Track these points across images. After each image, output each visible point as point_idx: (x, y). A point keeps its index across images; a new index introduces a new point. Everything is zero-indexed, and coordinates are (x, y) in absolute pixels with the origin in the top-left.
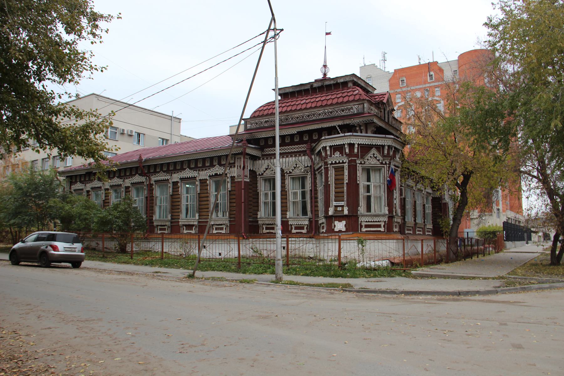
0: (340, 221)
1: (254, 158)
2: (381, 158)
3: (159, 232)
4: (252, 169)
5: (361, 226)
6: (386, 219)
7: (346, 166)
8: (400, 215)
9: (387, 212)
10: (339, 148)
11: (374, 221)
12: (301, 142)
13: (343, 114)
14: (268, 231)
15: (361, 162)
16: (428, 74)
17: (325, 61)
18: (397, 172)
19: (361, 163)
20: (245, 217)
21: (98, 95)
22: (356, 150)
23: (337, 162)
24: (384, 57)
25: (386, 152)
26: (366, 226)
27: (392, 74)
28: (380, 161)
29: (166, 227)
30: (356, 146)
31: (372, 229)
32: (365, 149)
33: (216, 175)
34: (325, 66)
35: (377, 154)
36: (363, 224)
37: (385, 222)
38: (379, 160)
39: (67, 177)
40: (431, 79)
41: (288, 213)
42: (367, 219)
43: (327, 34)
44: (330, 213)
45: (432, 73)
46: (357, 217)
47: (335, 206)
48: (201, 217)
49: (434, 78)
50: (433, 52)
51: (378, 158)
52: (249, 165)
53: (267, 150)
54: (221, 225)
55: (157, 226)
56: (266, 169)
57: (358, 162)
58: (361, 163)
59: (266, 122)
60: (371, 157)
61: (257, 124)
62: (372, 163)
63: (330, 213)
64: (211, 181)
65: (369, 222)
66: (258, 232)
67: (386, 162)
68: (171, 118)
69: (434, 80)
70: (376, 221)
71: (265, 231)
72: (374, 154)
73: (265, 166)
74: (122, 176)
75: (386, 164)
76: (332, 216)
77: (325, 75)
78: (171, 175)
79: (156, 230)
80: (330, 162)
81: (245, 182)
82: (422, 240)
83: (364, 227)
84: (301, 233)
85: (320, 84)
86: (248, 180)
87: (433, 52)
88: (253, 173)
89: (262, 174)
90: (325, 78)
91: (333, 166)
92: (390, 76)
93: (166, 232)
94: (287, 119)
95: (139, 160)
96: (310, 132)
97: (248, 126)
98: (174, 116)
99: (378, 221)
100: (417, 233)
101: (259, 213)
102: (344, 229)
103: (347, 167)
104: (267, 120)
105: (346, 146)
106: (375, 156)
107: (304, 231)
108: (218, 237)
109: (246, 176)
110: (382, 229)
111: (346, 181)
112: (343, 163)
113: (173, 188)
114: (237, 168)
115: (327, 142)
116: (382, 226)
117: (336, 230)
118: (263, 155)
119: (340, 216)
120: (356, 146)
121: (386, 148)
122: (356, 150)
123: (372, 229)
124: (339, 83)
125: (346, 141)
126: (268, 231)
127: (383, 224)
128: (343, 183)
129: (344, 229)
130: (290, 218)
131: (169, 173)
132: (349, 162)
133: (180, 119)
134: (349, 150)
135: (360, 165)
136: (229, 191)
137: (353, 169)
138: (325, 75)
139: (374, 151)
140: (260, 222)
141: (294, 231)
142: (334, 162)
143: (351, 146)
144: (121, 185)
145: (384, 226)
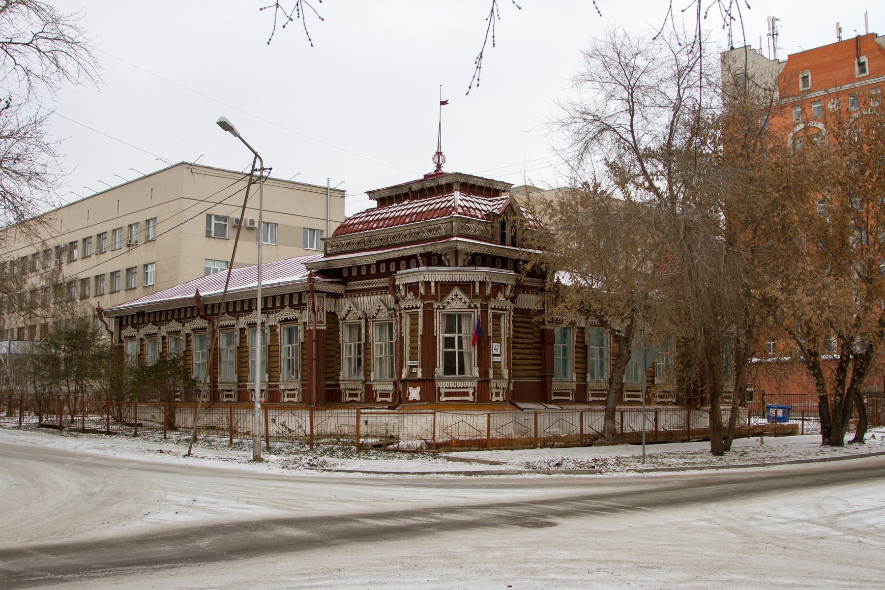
0: (414, 387)
1: (336, 296)
2: (468, 300)
3: (225, 400)
4: (329, 311)
5: (440, 394)
6: (475, 384)
7: (421, 311)
8: (506, 377)
9: (477, 375)
10: (412, 288)
11: (457, 388)
12: (379, 275)
13: (431, 235)
14: (351, 399)
15: (438, 306)
16: (856, 62)
17: (439, 146)
18: (503, 317)
19: (438, 308)
20: (318, 380)
21: (191, 165)
22: (433, 291)
23: (411, 306)
24: (773, 28)
25: (477, 291)
26: (447, 394)
27: (783, 65)
28: (467, 304)
29: (296, 392)
30: (433, 284)
31: (455, 398)
32: (445, 288)
33: (286, 320)
34: (439, 154)
35: (461, 294)
36: (443, 391)
37: (474, 388)
38: (465, 303)
39: (116, 318)
40: (863, 71)
41: (372, 374)
42: (447, 384)
43: (443, 103)
44: (404, 376)
45: (864, 59)
46: (433, 381)
47: (410, 366)
48: (271, 379)
49: (867, 69)
50: (866, 15)
51: (463, 300)
52: (328, 305)
53: (350, 283)
54: (293, 390)
55: (223, 391)
56: (349, 311)
57: (435, 306)
58: (438, 308)
59: (348, 244)
60: (452, 299)
61: (337, 246)
62: (456, 307)
63: (404, 376)
64: (282, 328)
65: (450, 388)
66: (339, 401)
67: (475, 305)
68: (327, 191)
69: (867, 73)
70: (460, 388)
71: (348, 399)
72: (457, 295)
73: (346, 308)
74: (182, 319)
75: (475, 307)
76: (405, 380)
77: (439, 166)
78: (238, 319)
79: (221, 396)
80: (403, 307)
81: (318, 331)
82: (489, 414)
83: (443, 395)
84: (386, 402)
85: (419, 186)
86: (325, 328)
87: (866, 15)
88: (332, 317)
89: (344, 319)
90: (438, 174)
91: (407, 311)
92: (781, 69)
93: (233, 400)
94: (370, 241)
95: (195, 298)
96: (388, 262)
97: (328, 249)
98: (332, 186)
99: (464, 388)
100: (626, 399)
101: (341, 373)
102: (418, 399)
103: (422, 313)
104: (349, 241)
105: (420, 285)
106: (459, 297)
107: (389, 399)
108: (290, 407)
109: (321, 322)
110: (470, 398)
111: (420, 333)
112: (416, 308)
113: (240, 338)
114: (323, 308)
115: (404, 277)
116: (471, 393)
117: (411, 399)
118: (347, 291)
119: (414, 380)
120: (433, 284)
121: (477, 285)
122: (433, 291)
123: (455, 398)
124: (442, 185)
125: (420, 278)
126: (351, 399)
127: (471, 391)
128: (417, 336)
129: (418, 399)
130: (374, 381)
131: (235, 316)
132: (425, 306)
133: (344, 191)
134: (426, 290)
135: (438, 311)
136: (302, 343)
137: (429, 316)
138: (439, 166)
139: (456, 291)
140: (342, 387)
141: (379, 399)
142: (407, 307)
143: (427, 284)
144: (180, 331)
145: (473, 394)
